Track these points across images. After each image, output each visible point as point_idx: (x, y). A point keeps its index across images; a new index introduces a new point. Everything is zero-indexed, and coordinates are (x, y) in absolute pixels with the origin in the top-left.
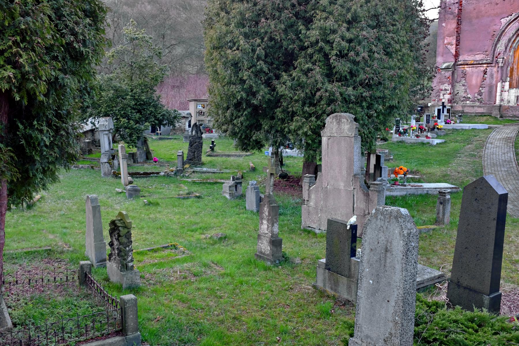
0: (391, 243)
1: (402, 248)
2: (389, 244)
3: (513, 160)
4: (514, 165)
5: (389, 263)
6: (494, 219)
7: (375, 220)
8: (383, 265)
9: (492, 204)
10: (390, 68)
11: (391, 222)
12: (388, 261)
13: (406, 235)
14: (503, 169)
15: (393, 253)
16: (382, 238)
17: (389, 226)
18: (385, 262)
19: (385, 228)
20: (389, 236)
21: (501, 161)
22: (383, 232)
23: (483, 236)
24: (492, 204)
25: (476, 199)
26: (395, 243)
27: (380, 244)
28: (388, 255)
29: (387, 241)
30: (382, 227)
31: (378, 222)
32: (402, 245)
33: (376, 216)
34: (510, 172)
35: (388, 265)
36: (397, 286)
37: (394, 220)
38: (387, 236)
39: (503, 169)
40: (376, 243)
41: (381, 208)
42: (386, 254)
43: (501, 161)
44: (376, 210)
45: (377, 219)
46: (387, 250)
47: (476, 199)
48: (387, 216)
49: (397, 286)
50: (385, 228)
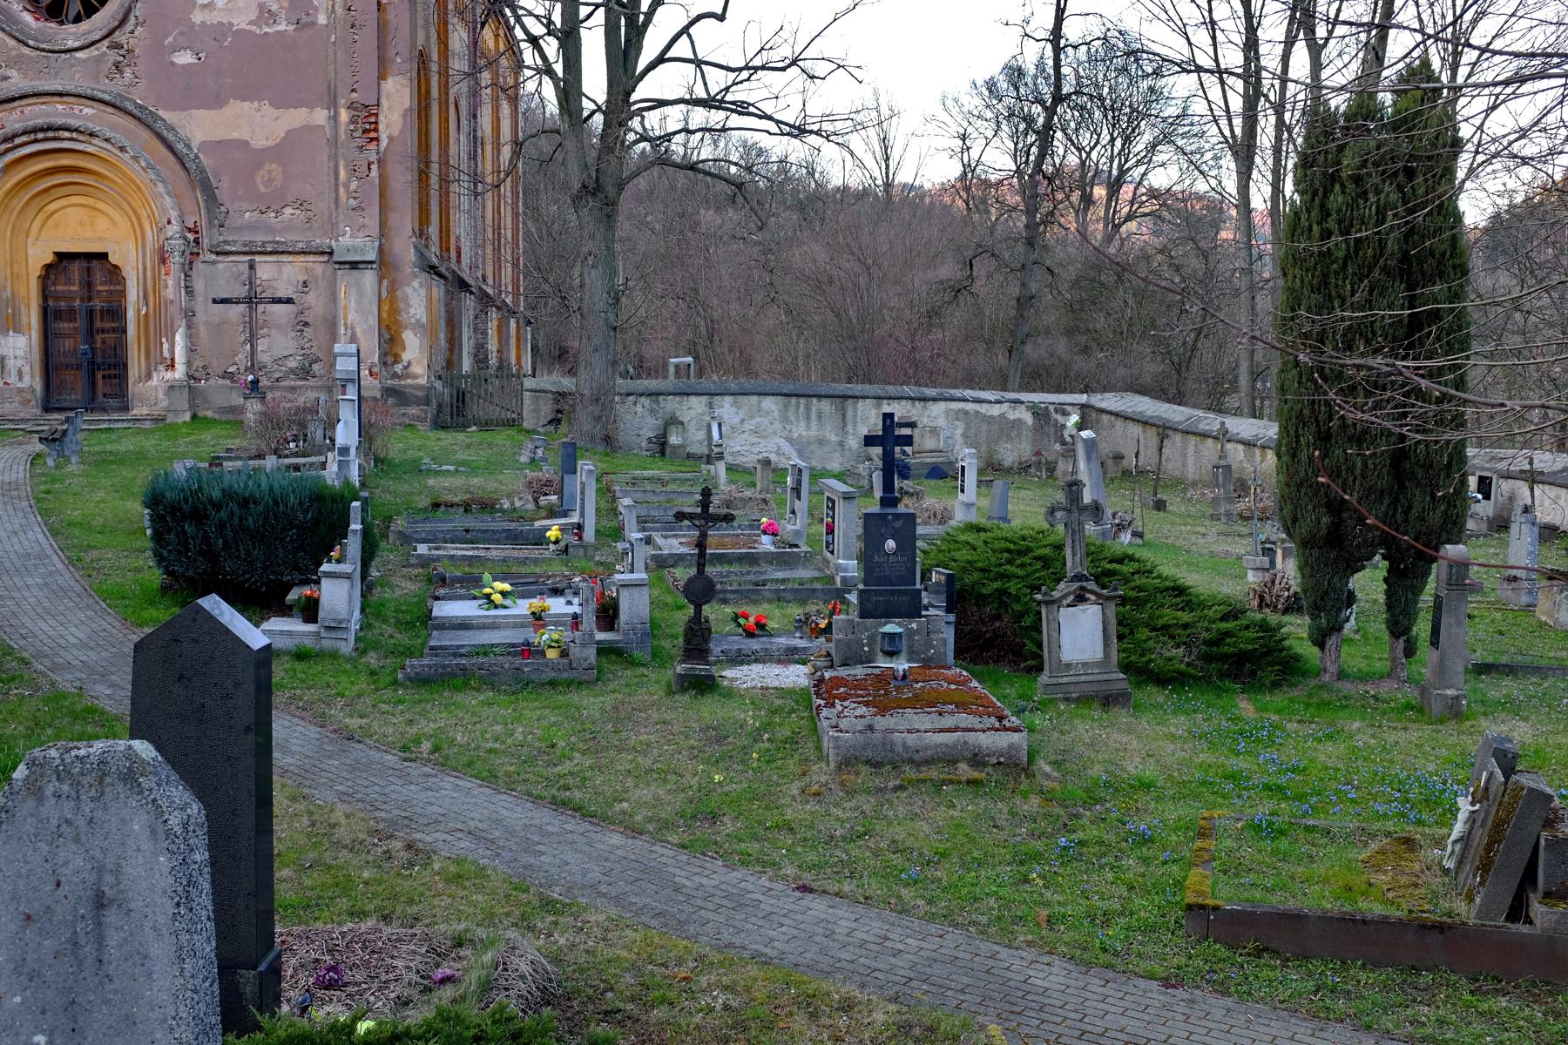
0: (117, 871)
1: (171, 880)
2: (109, 878)
3: (50, 552)
4: (61, 566)
5: (120, 946)
6: (248, 729)
7: (31, 803)
8: (89, 962)
9: (237, 685)
10: (390, 343)
11: (108, 796)
12: (113, 938)
13: (178, 830)
14: (29, 581)
15: (133, 905)
16: (73, 862)
17: (99, 814)
18: (100, 942)
19: (81, 822)
20: (104, 851)
21: (13, 556)
22: (77, 840)
23: (216, 789)
24: (237, 685)
25: (182, 677)
26: (134, 869)
27: (64, 889)
28: (111, 916)
29: (100, 869)
30: (68, 822)
31: (50, 809)
32: (165, 871)
33: (34, 788)
34: (54, 587)
35: (113, 952)
36: (165, 1020)
37: (120, 788)
38: (98, 854)
39: (29, 581)
40: (50, 887)
41: (53, 753)
42: (97, 916)
43: (13, 556)
44: (32, 764)
45: (40, 799)
46: (100, 903)
47: (182, 677)
48: (85, 781)
49: (165, 1020)
50: (81, 822)
